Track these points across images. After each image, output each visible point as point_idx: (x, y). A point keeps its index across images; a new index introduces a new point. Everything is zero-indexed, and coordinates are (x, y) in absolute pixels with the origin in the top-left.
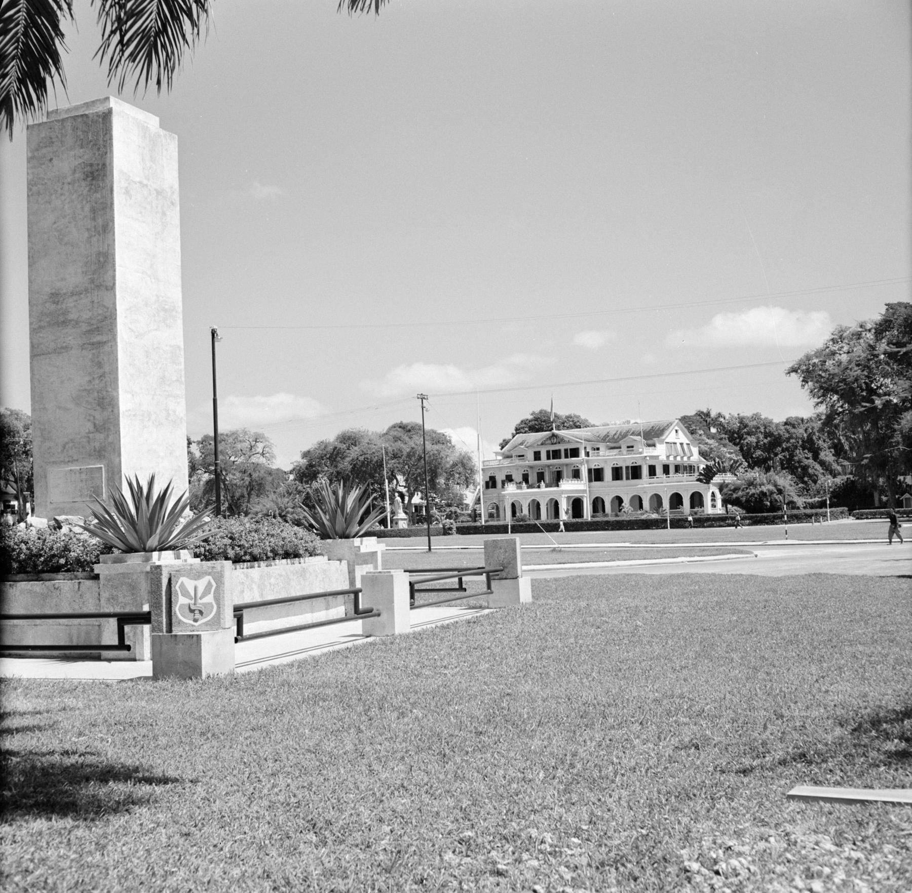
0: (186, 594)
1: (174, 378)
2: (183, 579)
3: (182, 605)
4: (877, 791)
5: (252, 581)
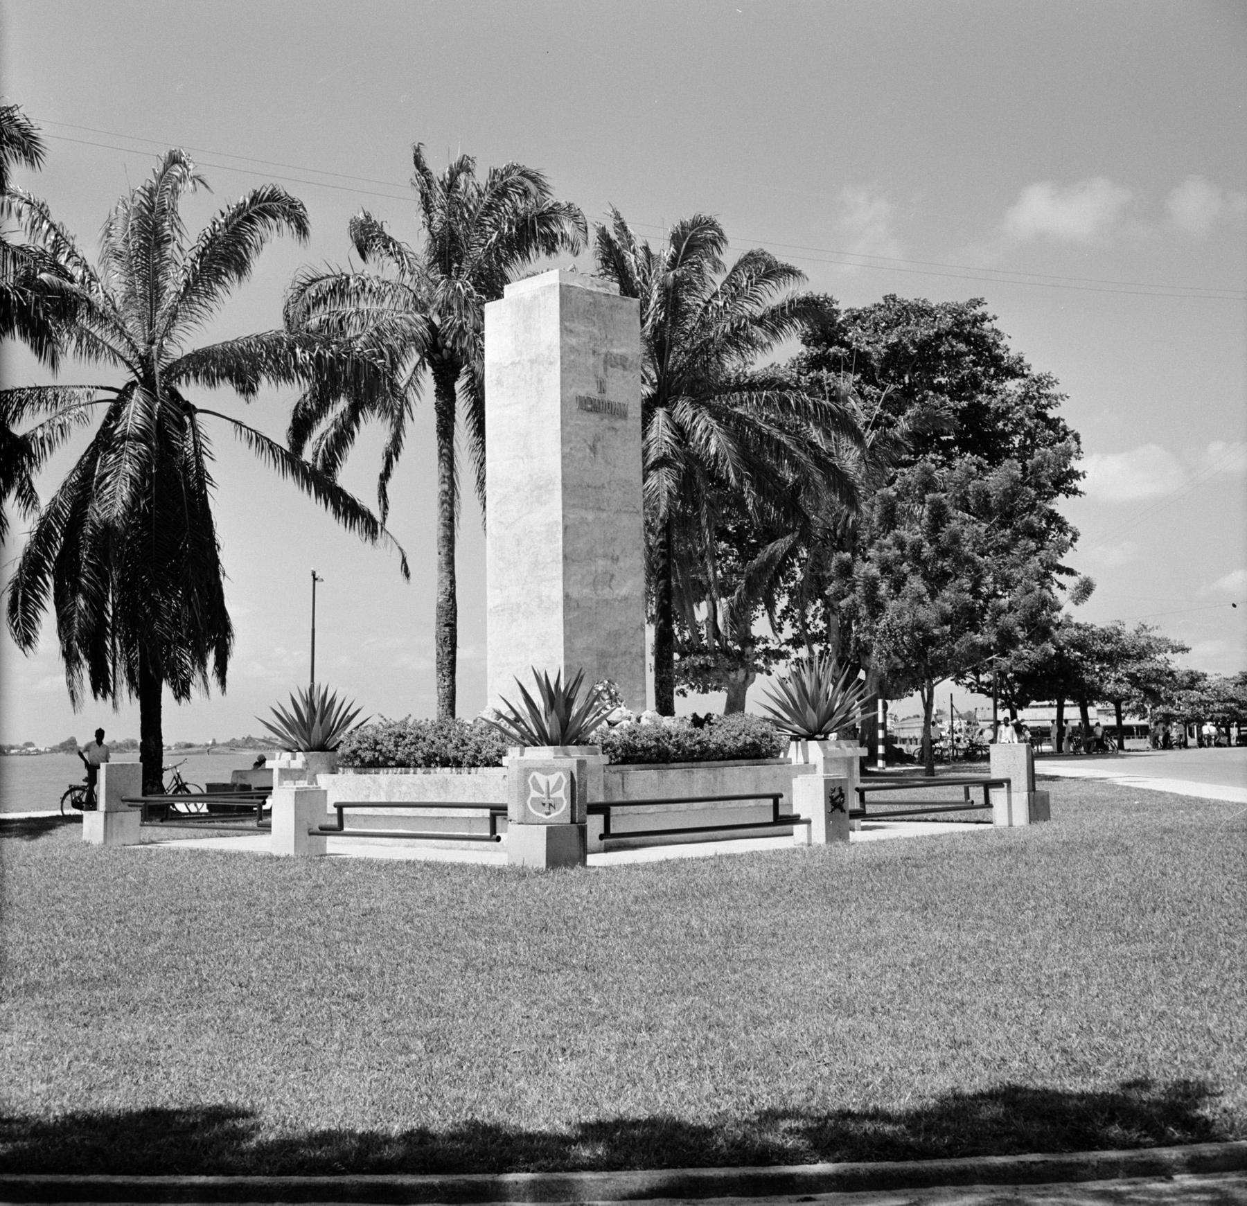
0: (538, 788)
1: (549, 560)
2: (535, 774)
3: (533, 799)
4: (927, 833)
5: (380, 786)
